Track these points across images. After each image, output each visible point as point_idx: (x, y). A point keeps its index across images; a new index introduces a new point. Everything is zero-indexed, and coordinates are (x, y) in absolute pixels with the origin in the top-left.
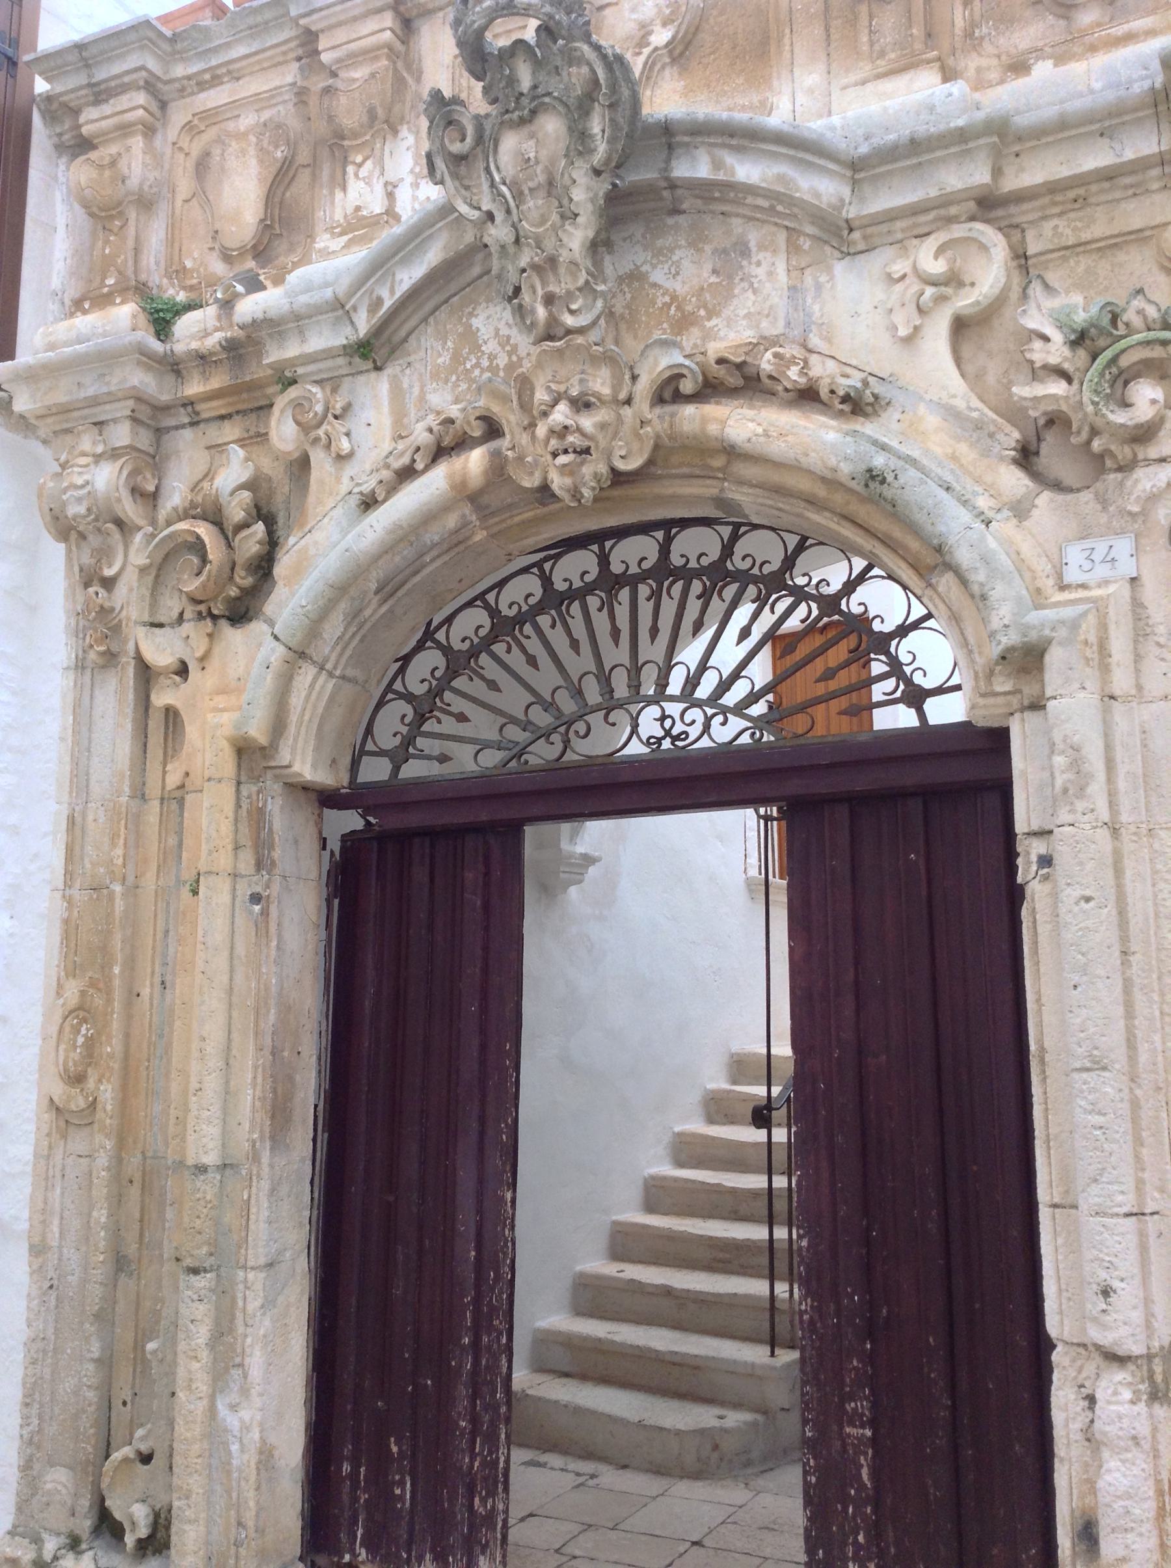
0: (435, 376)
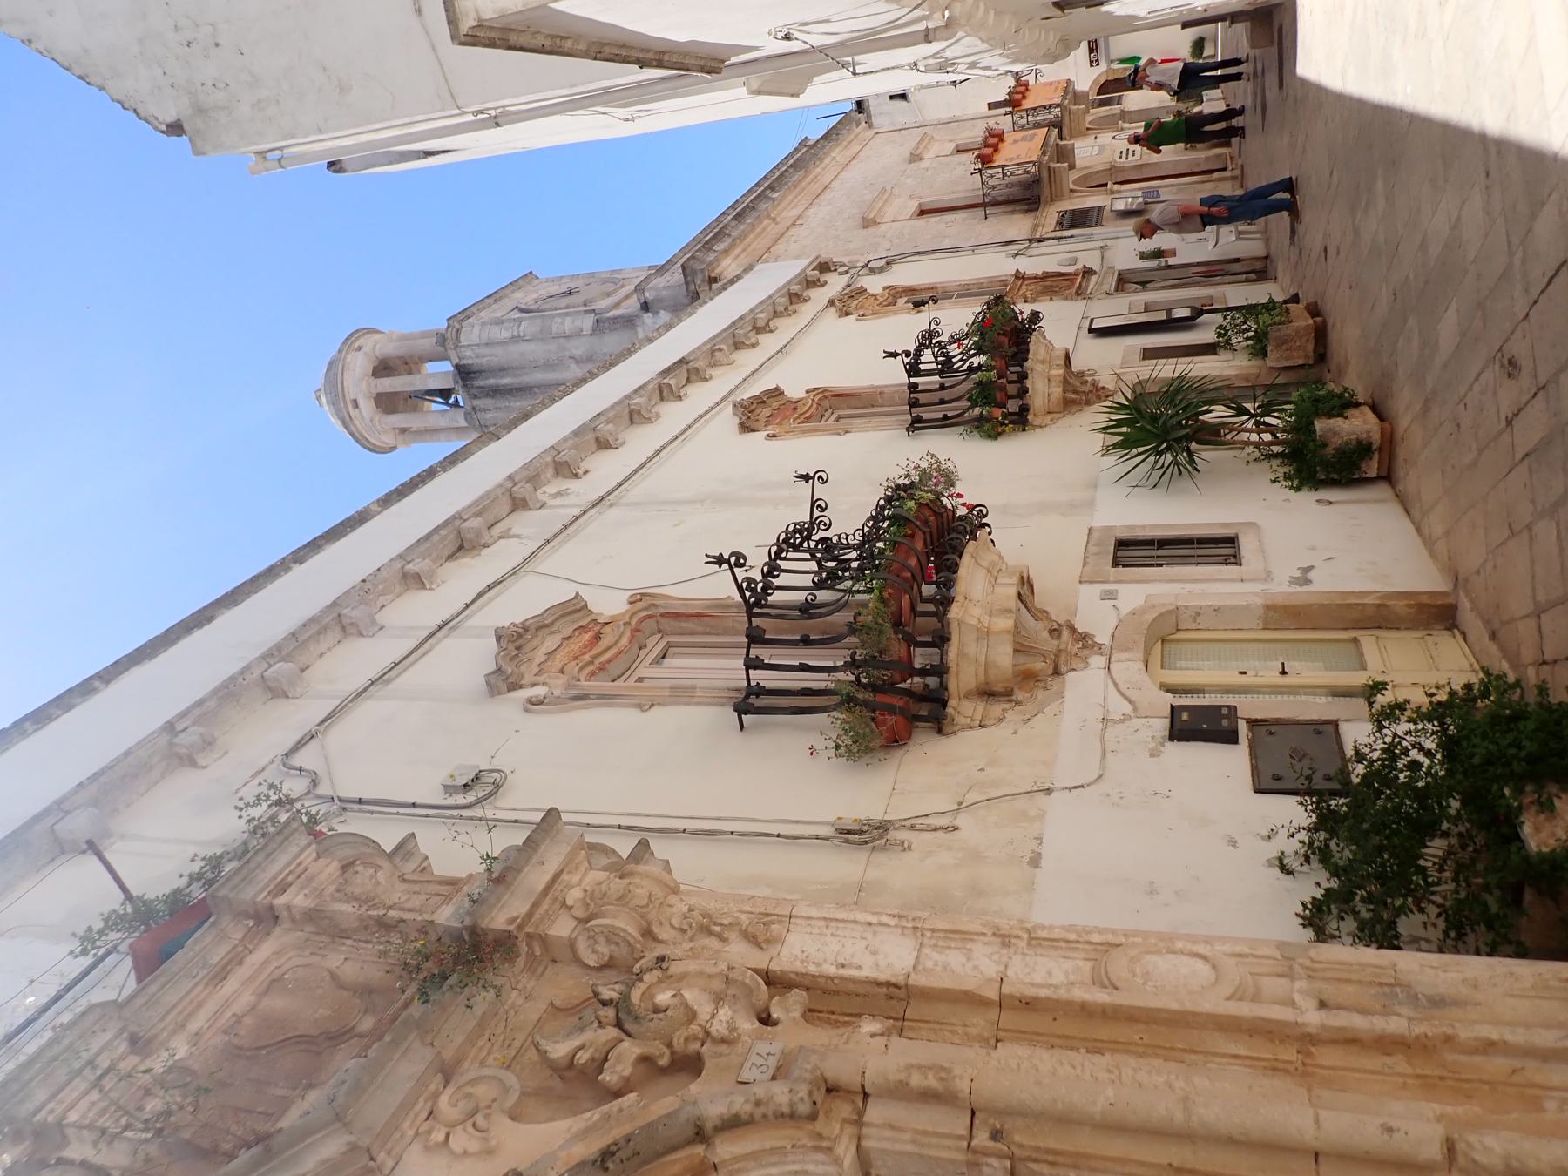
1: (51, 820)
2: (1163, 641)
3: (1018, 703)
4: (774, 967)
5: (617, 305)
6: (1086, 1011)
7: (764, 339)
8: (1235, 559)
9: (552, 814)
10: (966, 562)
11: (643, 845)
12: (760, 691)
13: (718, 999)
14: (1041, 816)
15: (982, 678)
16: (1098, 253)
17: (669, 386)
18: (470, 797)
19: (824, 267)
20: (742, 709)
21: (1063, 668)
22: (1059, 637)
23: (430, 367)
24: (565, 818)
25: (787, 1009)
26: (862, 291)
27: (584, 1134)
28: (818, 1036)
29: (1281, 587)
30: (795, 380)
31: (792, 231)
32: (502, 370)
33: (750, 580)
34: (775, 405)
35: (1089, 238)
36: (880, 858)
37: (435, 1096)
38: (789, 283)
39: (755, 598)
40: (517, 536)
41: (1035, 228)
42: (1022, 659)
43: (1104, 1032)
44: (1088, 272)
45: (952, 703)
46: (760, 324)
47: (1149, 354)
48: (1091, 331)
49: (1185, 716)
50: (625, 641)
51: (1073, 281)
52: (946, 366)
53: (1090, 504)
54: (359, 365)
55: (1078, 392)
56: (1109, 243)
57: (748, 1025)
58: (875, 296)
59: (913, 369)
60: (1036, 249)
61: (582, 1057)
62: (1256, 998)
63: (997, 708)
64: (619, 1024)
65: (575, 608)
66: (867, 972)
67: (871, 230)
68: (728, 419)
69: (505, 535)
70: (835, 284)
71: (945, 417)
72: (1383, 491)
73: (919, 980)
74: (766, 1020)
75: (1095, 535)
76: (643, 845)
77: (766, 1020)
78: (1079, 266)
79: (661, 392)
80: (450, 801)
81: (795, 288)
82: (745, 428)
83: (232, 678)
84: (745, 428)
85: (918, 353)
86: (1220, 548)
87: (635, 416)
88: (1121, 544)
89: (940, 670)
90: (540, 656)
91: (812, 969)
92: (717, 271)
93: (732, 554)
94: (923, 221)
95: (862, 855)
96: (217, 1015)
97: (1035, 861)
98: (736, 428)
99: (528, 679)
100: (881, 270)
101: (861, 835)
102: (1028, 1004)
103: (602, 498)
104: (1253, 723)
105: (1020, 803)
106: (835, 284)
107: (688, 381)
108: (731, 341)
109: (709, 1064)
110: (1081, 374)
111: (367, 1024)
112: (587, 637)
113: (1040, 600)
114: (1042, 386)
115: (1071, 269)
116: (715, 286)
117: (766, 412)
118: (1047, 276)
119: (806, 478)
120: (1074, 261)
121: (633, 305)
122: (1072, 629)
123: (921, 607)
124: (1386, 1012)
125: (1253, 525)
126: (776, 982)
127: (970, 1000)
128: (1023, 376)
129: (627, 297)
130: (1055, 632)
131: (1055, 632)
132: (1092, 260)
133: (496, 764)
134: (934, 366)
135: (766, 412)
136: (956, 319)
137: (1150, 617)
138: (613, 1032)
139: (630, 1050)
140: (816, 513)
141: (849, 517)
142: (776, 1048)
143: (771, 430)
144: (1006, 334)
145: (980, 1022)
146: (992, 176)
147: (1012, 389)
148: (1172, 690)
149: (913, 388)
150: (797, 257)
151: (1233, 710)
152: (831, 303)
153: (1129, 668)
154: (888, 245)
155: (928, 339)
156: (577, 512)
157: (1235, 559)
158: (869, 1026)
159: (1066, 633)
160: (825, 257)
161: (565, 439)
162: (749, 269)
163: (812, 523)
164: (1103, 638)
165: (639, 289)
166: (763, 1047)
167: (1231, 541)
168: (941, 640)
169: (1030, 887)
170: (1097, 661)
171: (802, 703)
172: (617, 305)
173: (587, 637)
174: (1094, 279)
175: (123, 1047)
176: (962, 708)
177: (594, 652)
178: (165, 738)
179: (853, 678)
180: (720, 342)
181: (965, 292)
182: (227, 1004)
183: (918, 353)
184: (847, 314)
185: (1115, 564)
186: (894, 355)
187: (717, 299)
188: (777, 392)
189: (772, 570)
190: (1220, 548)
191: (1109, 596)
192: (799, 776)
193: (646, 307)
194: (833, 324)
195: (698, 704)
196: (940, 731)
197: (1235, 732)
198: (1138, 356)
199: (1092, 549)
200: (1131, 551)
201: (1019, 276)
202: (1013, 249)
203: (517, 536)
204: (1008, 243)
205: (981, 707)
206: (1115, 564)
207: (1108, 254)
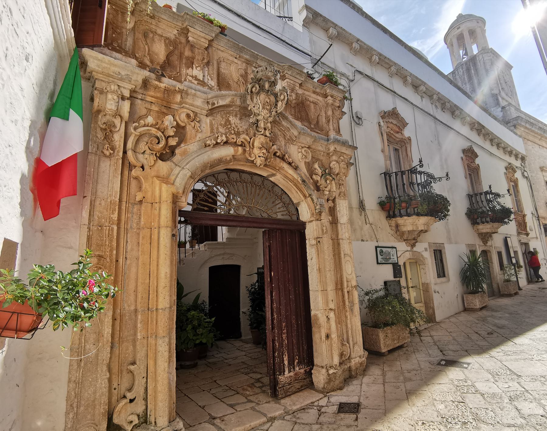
0: (221, 125)
1: (332, 25)
3: (396, 232)
4: (336, 199)
5: (503, 99)
6: (339, 254)
7: (495, 148)
8: (439, 276)
9: (356, 148)
10: (430, 218)
11: (353, 164)
12: (390, 177)
13: (330, 191)
14: (372, 241)
16: (535, 236)
18: (355, 118)
19: (523, 159)
20: (385, 174)
24: (356, 151)
25: (331, 204)
26: (515, 172)
27: (305, 175)
28: (327, 210)
29: (433, 287)
30: (482, 160)
32: (476, 70)
33: (417, 169)
34: (472, 157)
35: (541, 234)
36: (358, 210)
37: (305, 147)
39: (413, 171)
40: (422, 100)
42: (407, 232)
43: (337, 257)
44: (527, 234)
45: (394, 219)
46: (500, 145)
48: (506, 237)
50: (398, 140)
51: (524, 230)
52: (489, 201)
53: (451, 243)
55: (485, 237)
57: (326, 197)
58: (514, 175)
59: (486, 193)
61: (316, 171)
62: (347, 281)
63: (394, 228)
64: (322, 175)
65: (405, 124)
66: (339, 216)
67: (539, 170)
68: (466, 145)
69: (422, 97)
70: (517, 163)
72: (461, 308)
73: (339, 225)
74: (328, 200)
75: (442, 245)
76: (353, 164)
77: (328, 200)
78: (529, 232)
80: (354, 113)
81: (514, 152)
82: (464, 151)
83: (372, 48)
84: (464, 151)
85: (492, 194)
86: (441, 272)
88: (440, 251)
89: (401, 216)
90: (390, 121)
91: (338, 206)
92: (519, 127)
95: (358, 206)
96: (308, 96)
97: (362, 240)
98: (463, 148)
99: (385, 120)
100: (524, 176)
101: (362, 206)
102: (339, 244)
103: (437, 119)
104: (399, 281)
105: (374, 236)
106: (517, 163)
107: (477, 130)
109: (319, 193)
110: (491, 236)
111: (312, 126)
112: (398, 130)
114: (485, 228)
116: (513, 128)
117: (470, 155)
118: (525, 224)
119: (447, 175)
120: (531, 230)
121: (503, 103)
123: (416, 209)
124: (349, 302)
125: (449, 280)
126: (334, 201)
127: (337, 235)
128: (487, 222)
129: (506, 101)
130: (414, 239)
132: (532, 234)
133: (364, 121)
135: (470, 155)
136: (507, 202)
138: (321, 175)
139: (318, 178)
141: (437, 188)
142: (324, 203)
143: (464, 158)
144: (502, 216)
145: (334, 237)
147: (484, 220)
148: (404, 263)
149: (481, 194)
150: (526, 150)
153: (408, 255)
154: (534, 175)
155: (498, 195)
156: (432, 114)
157: (439, 276)
158: (330, 218)
159: (414, 241)
160: (527, 158)
161: (453, 103)
162: (520, 136)
163: (435, 178)
164: (415, 249)
165: (510, 104)
166: (324, 201)
167: (444, 276)
168: (409, 215)
169: (358, 240)
172: (503, 99)
173: (398, 130)
174: (525, 236)
175: (300, 82)
176: (393, 222)
177: (394, 133)
178: (356, 40)
181: (518, 202)
182: (310, 96)
183: (492, 194)
184: (506, 169)
185: (434, 250)
186: (490, 187)
187: (508, 130)
188: (477, 156)
189: (420, 173)
190: (441, 272)
191: (426, 250)
192: (373, 191)
193: (503, 108)
196: (387, 217)
198: (498, 250)
199: (438, 245)
201: (524, 216)
203: (422, 100)
205: (394, 225)
206: (434, 250)
207: (535, 239)
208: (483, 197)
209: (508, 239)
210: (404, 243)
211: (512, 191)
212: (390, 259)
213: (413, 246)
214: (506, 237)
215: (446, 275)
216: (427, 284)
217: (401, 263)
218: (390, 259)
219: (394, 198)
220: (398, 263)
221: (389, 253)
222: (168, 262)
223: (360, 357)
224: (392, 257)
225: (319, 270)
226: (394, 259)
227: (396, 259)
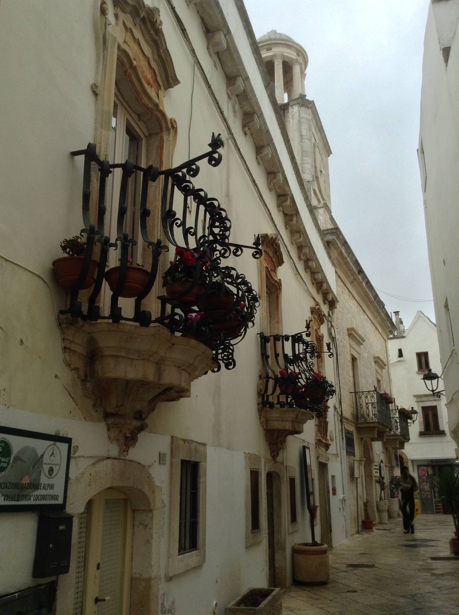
2: (126, 500)
15: (107, 353)
16: (335, 453)
17: (286, 201)
20: (90, 153)
21: (111, 421)
22: (136, 418)
23: (286, 95)
31: (347, 291)
38: (328, 283)
41: (347, 419)
44: (327, 446)
47: (292, 480)
49: (62, 527)
53: (219, 445)
54: (291, 54)
56: (339, 459)
58: (319, 328)
60: (337, 418)
67: (346, 332)
68: (269, 231)
70: (325, 309)
71: (267, 357)
75: (201, 448)
78: (330, 442)
79: (283, 196)
87: (272, 176)
93: (220, 157)
94: (349, 358)
106: (325, 309)
108: (303, 244)
113: (163, 406)
115: (328, 438)
122: (141, 428)
131: (139, 415)
132: (332, 449)
134: (297, 353)
137: (146, 490)
140: (232, 248)
146: (372, 397)
151: (66, 570)
152: (317, 304)
159: (137, 423)
160: (338, 305)
170: (114, 450)
171: (91, 202)
179: (112, 241)
180: (304, 238)
184: (312, 312)
191: (161, 457)
194: (308, 304)
195: (96, 130)
197: (43, 576)
200: (191, 473)
202: (338, 406)
204: (340, 403)
205: (81, 350)
208: (288, 345)
209: (307, 451)
210: (102, 426)
211: (174, 123)
212: (35, 486)
213: (130, 440)
214: (304, 448)
215: (200, 544)
216: (149, 580)
217: (75, 507)
218: (35, 486)
219: (106, 243)
220: (63, 506)
221: (38, 461)
222: (261, 483)
223: (393, 496)
224: (44, 480)
225: (329, 493)
226: (51, 488)
227: (59, 490)
